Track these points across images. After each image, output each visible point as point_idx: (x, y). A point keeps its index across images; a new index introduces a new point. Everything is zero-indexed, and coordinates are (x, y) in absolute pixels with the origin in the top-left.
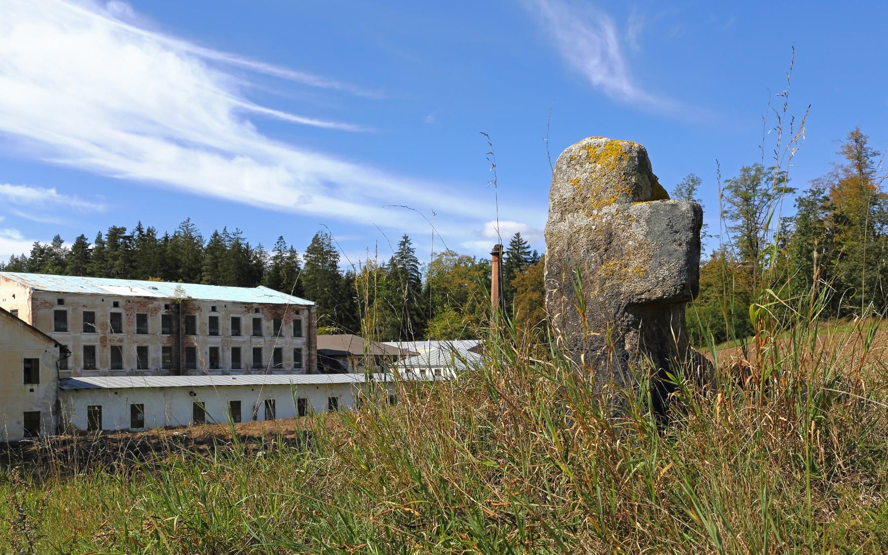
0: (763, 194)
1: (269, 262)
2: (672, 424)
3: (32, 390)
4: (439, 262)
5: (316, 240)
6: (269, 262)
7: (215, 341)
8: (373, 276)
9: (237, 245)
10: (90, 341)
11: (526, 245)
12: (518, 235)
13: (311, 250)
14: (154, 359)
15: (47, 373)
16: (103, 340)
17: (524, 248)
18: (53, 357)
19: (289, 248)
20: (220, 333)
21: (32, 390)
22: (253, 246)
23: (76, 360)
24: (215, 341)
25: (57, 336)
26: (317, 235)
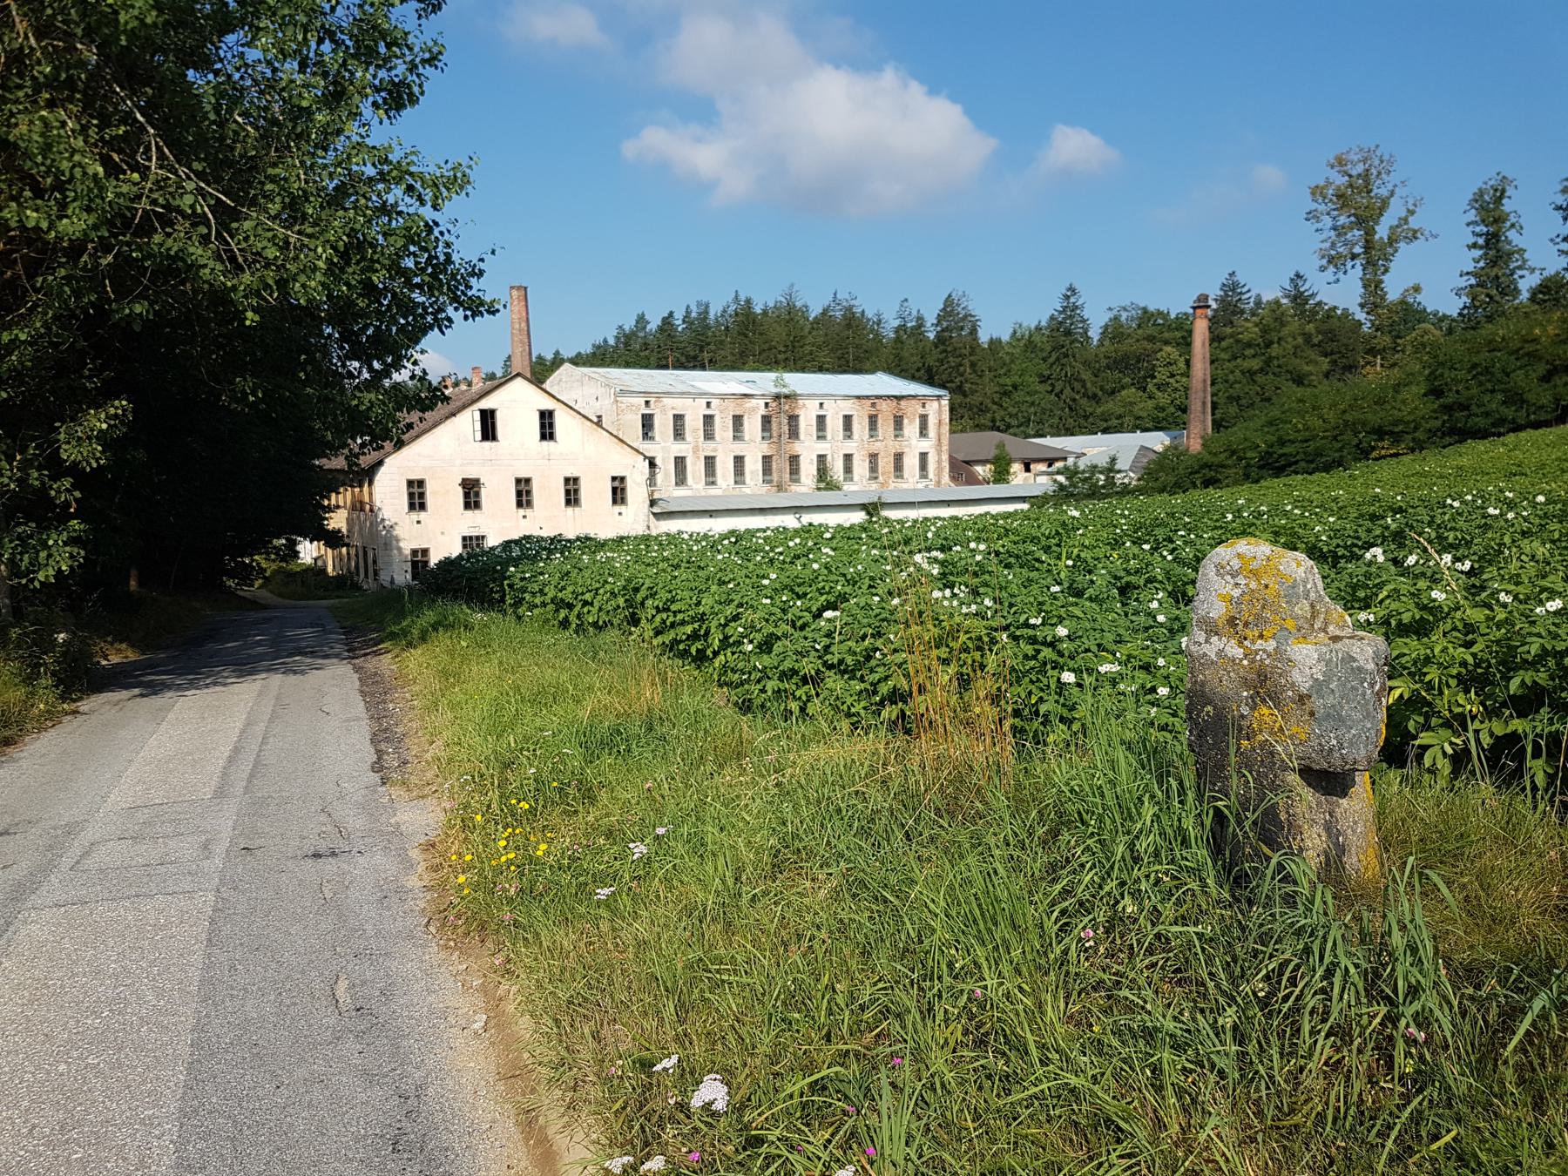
0: (407, 683)
1: (888, 332)
2: (81, 425)
3: (524, 517)
4: (1116, 318)
5: (949, 301)
6: (888, 332)
7: (822, 447)
8: (1027, 343)
9: (850, 309)
10: (681, 451)
11: (1244, 290)
12: (1232, 274)
13: (940, 319)
14: (752, 472)
15: (637, 492)
16: (696, 450)
17: (1241, 293)
18: (642, 473)
19: (914, 313)
20: (829, 437)
21: (524, 517)
22: (870, 314)
23: (667, 475)
24: (822, 447)
25: (548, 404)
26: (950, 296)
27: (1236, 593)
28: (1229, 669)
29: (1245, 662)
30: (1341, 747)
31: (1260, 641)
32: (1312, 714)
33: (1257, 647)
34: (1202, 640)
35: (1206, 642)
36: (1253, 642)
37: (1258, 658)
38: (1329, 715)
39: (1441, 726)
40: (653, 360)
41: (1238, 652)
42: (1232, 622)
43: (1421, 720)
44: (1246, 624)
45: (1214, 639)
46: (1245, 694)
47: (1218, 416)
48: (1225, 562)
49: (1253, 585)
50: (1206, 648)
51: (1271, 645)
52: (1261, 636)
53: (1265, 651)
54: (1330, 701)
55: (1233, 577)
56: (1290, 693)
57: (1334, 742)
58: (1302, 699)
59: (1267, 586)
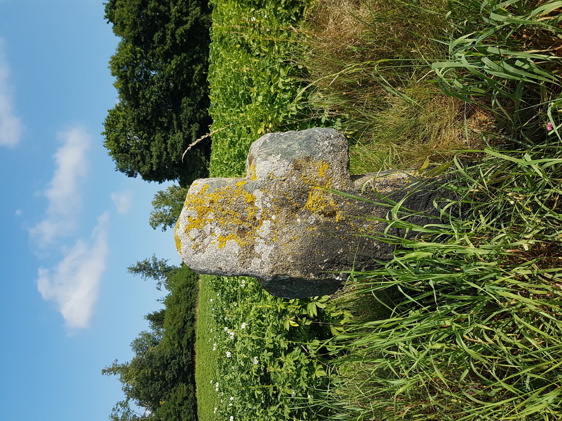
27: (218, 231)
28: (280, 233)
29: (274, 217)
30: (329, 138)
31: (256, 204)
32: (308, 159)
33: (260, 206)
34: (258, 261)
35: (260, 257)
36: (257, 211)
37: (269, 205)
38: (307, 146)
39: (306, 310)
40: (408, 293)
41: (266, 224)
42: (242, 232)
43: (304, 319)
44: (243, 219)
45: (257, 249)
46: (298, 220)
47: (182, 388)
48: (193, 243)
49: (211, 216)
50: (265, 257)
51: (258, 194)
52: (252, 203)
53: (263, 199)
54: (296, 146)
55: (205, 237)
56: (294, 178)
57: (326, 143)
58: (297, 168)
59: (212, 202)
